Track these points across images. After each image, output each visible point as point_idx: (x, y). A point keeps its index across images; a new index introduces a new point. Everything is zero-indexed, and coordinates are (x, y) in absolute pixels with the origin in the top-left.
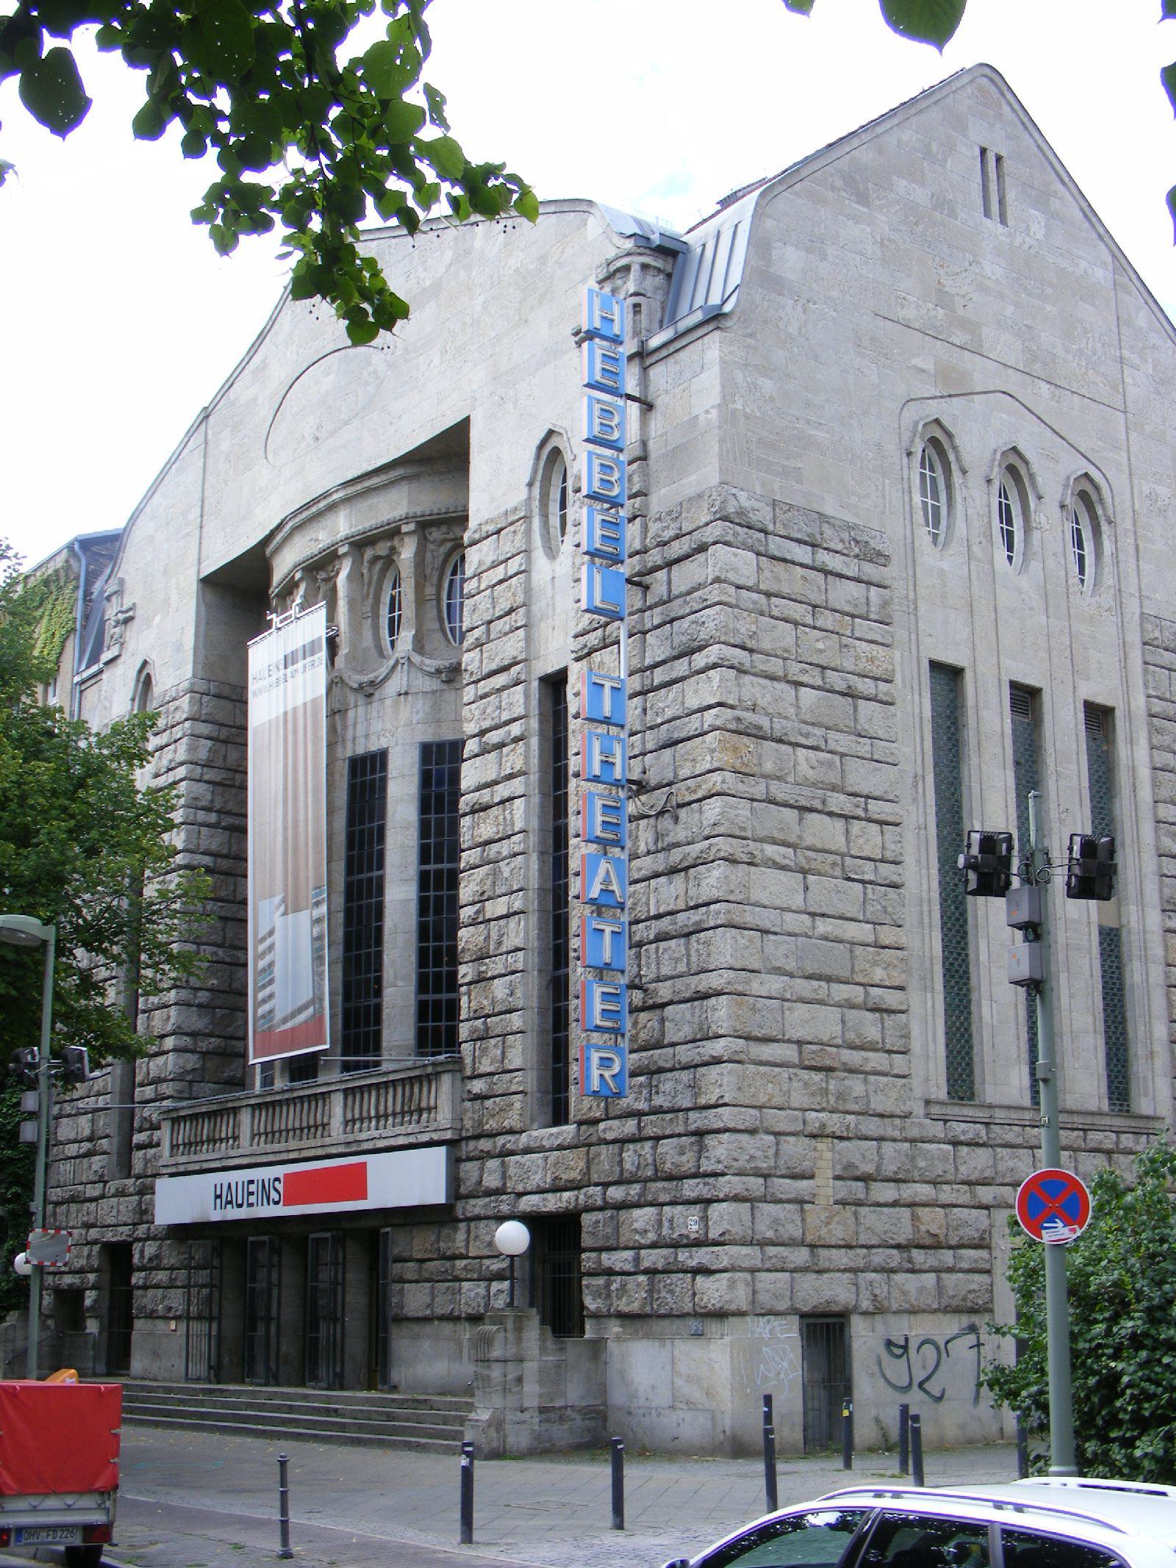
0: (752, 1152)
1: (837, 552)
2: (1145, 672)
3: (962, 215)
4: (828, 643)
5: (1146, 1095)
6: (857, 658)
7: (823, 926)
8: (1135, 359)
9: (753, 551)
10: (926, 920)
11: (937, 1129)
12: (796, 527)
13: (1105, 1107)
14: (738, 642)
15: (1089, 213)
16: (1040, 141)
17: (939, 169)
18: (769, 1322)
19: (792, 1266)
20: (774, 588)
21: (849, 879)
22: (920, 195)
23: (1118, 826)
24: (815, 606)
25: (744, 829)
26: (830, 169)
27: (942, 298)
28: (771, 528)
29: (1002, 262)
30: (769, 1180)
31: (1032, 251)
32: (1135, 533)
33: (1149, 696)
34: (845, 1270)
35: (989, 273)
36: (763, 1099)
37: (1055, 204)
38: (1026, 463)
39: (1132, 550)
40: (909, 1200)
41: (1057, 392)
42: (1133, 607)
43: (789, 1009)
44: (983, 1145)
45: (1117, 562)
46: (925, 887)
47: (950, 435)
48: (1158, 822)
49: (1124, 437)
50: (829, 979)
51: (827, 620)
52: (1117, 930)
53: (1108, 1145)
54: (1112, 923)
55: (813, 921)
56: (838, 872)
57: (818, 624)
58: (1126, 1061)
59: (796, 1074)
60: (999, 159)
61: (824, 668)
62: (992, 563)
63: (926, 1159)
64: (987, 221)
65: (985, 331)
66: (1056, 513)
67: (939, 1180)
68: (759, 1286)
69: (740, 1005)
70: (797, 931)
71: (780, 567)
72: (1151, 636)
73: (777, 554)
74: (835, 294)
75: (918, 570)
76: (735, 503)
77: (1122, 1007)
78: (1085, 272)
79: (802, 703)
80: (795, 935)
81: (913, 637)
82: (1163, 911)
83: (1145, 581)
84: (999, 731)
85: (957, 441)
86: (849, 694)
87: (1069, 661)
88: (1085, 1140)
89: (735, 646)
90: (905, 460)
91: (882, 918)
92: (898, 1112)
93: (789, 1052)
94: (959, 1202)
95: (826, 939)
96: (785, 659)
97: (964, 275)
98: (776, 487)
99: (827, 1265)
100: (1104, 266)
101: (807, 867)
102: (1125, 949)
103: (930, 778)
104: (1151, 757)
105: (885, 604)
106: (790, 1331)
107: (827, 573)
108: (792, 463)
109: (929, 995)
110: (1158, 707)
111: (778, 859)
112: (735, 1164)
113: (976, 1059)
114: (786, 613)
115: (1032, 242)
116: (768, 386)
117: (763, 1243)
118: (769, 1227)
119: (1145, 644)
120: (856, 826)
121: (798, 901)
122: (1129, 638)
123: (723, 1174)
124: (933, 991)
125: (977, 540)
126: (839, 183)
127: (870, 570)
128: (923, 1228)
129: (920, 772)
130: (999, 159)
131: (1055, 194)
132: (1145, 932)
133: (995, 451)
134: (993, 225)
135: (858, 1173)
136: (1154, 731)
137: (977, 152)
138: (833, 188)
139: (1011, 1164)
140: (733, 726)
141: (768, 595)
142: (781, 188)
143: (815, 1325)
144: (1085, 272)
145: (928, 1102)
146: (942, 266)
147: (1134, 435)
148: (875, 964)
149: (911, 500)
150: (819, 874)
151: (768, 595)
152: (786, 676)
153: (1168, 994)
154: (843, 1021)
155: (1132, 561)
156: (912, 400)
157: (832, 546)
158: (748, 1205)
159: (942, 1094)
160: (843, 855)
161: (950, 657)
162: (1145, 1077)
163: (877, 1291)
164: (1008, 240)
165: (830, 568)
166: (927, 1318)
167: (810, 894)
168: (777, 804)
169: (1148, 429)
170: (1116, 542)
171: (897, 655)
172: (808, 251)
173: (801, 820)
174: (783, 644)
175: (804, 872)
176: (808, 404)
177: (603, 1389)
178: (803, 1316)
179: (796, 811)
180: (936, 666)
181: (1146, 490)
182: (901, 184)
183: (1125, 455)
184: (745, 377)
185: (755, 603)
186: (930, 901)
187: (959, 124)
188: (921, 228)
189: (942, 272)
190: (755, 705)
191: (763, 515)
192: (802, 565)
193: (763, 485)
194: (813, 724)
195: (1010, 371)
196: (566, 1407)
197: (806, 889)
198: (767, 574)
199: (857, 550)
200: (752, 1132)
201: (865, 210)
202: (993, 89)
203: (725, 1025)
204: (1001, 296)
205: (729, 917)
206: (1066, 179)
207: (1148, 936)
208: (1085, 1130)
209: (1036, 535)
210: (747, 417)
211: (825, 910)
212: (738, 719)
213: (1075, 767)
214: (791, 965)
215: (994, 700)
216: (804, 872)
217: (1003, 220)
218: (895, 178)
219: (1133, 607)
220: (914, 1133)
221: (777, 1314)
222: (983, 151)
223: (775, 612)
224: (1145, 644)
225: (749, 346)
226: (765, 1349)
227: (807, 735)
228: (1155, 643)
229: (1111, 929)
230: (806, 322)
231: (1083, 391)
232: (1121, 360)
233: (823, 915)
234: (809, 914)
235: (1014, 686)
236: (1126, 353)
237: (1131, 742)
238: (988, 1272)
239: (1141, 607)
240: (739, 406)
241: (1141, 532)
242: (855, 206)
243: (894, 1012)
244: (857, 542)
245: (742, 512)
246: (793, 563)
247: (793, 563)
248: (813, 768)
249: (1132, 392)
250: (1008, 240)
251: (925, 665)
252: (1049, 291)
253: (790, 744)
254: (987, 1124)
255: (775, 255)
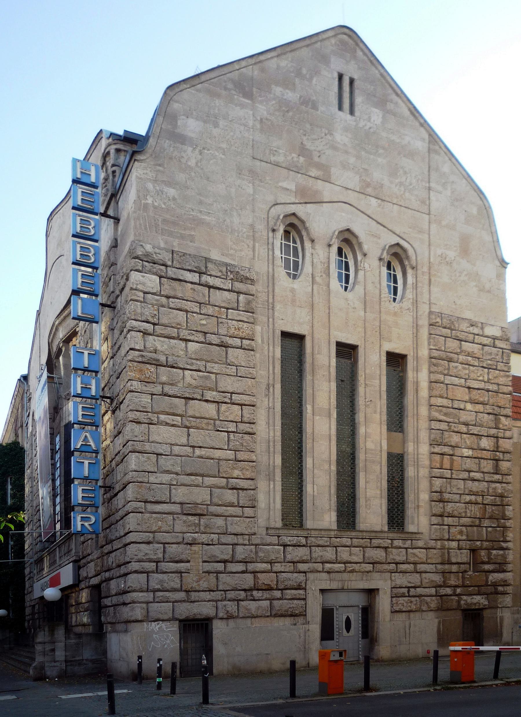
0: (147, 552)
1: (217, 277)
2: (429, 338)
3: (322, 108)
4: (208, 321)
5: (413, 523)
6: (229, 328)
7: (198, 452)
8: (440, 188)
9: (157, 275)
10: (272, 449)
11: (275, 540)
12: (188, 264)
13: (386, 528)
14: (143, 318)
15: (414, 112)
16: (382, 71)
17: (307, 83)
18: (158, 624)
19: (173, 600)
20: (172, 293)
21: (218, 431)
22: (291, 96)
23: (406, 408)
24: (200, 304)
25: (145, 407)
26: (225, 78)
27: (303, 151)
28: (169, 263)
29: (350, 135)
30: (159, 564)
31: (372, 130)
32: (429, 273)
33: (431, 349)
34: (209, 601)
35: (339, 140)
36: (154, 529)
37: (390, 106)
38: (356, 237)
39: (427, 282)
40: (252, 570)
41: (383, 203)
42: (424, 309)
43: (174, 489)
44: (304, 546)
45: (416, 286)
46: (272, 434)
47: (303, 222)
48: (431, 406)
49: (427, 227)
50: (202, 476)
51: (210, 310)
52: (402, 454)
53: (349, 544)
54: (397, 450)
55: (484, 475)
56: (210, 427)
57: (202, 312)
58: (403, 510)
59: (178, 517)
60: (352, 81)
61: (205, 333)
62: (328, 286)
63: (264, 552)
64: (340, 113)
65: (333, 170)
66: (376, 263)
67: (273, 561)
68: (150, 609)
69: (140, 487)
70: (182, 454)
71: (176, 284)
72: (434, 321)
73: (174, 277)
74: (224, 146)
75: (276, 288)
76: (142, 249)
77: (403, 487)
78: (409, 143)
79: (189, 349)
80: (181, 456)
81: (271, 320)
82: (431, 445)
83: (433, 296)
84: (328, 364)
85: (307, 225)
86: (223, 345)
87: (378, 333)
88: (371, 543)
89: (143, 321)
90: (271, 234)
91: (240, 448)
92: (247, 533)
93: (176, 508)
94: (286, 570)
95: (202, 457)
96: (178, 329)
97: (320, 140)
98: (175, 244)
99: (197, 599)
100: (423, 140)
101: (189, 425)
102: (405, 462)
103: (278, 386)
104: (429, 377)
105: (249, 303)
106: (173, 627)
107: (210, 287)
108: (187, 232)
109: (272, 483)
110: (435, 354)
111: (168, 422)
112: (136, 557)
113: (304, 510)
114: (179, 306)
115: (372, 125)
116: (172, 192)
117: (155, 591)
118: (157, 584)
119: (430, 325)
120: (223, 407)
121: (184, 440)
122: (420, 323)
123: (130, 562)
124: (274, 481)
125: (319, 275)
126: (230, 86)
127: (239, 286)
128: (260, 582)
129: (271, 382)
130: (352, 81)
131: (391, 101)
132: (418, 455)
133: (335, 231)
134: (345, 116)
135: (218, 560)
136: (431, 364)
137: (336, 75)
138: (226, 89)
139: (321, 554)
140: (140, 359)
141: (168, 297)
142: (185, 86)
143: (186, 624)
144: (409, 143)
145: (267, 529)
146: (305, 135)
147: (433, 226)
148: (234, 468)
149: (273, 253)
150: (198, 428)
151: (168, 297)
152: (179, 336)
153: (430, 482)
154: (211, 494)
155: (426, 287)
156: (277, 204)
157: (213, 273)
158: (146, 574)
159: (279, 524)
160: (215, 420)
161: (397, 348)
162: (412, 517)
163: (228, 609)
164: (354, 123)
165: (211, 284)
166: (263, 620)
167: (190, 437)
168: (170, 396)
169: (444, 223)
170: (416, 277)
171: (258, 328)
172: (205, 122)
173: (186, 404)
174: (177, 321)
175: (188, 428)
176: (201, 203)
177: (105, 652)
178: (180, 621)
179: (183, 400)
180: (285, 335)
181: (439, 252)
182: (278, 90)
183: (427, 236)
184: (154, 187)
185: (157, 300)
186: (274, 441)
187: (325, 59)
188: (291, 114)
189: (305, 138)
190: (156, 350)
191: (167, 257)
192: (192, 283)
193: (166, 243)
194: (197, 359)
195: (350, 192)
196: (83, 660)
197: (189, 435)
198: (166, 286)
199: (232, 276)
200: (149, 543)
201: (249, 102)
202: (351, 41)
203: (131, 496)
204: (346, 152)
205: (133, 447)
206: (399, 92)
207: (420, 456)
208: (371, 539)
209: (361, 273)
210: (155, 207)
211: (201, 445)
212: (142, 356)
213: (377, 381)
214: (178, 469)
215: (325, 351)
216: (188, 428)
217: (352, 112)
218: (273, 86)
219: (424, 309)
220: (258, 541)
221: (163, 620)
222: (341, 77)
223: (172, 305)
224: (430, 325)
225: (159, 171)
226: (154, 636)
227: (192, 364)
228: (437, 324)
229: (399, 454)
230: (201, 159)
231: (400, 203)
232: (429, 189)
233: (200, 447)
234: (191, 446)
235: (339, 344)
236: (433, 185)
237: (417, 370)
238: (304, 599)
239: (430, 308)
240: (150, 201)
241: (433, 272)
242: (242, 99)
243: (246, 489)
244: (231, 272)
245: (147, 255)
246: (186, 282)
247: (186, 282)
248: (195, 380)
249: (435, 205)
250: (354, 123)
251: (278, 334)
252: (381, 151)
253: (181, 369)
254: (306, 537)
255: (179, 123)
